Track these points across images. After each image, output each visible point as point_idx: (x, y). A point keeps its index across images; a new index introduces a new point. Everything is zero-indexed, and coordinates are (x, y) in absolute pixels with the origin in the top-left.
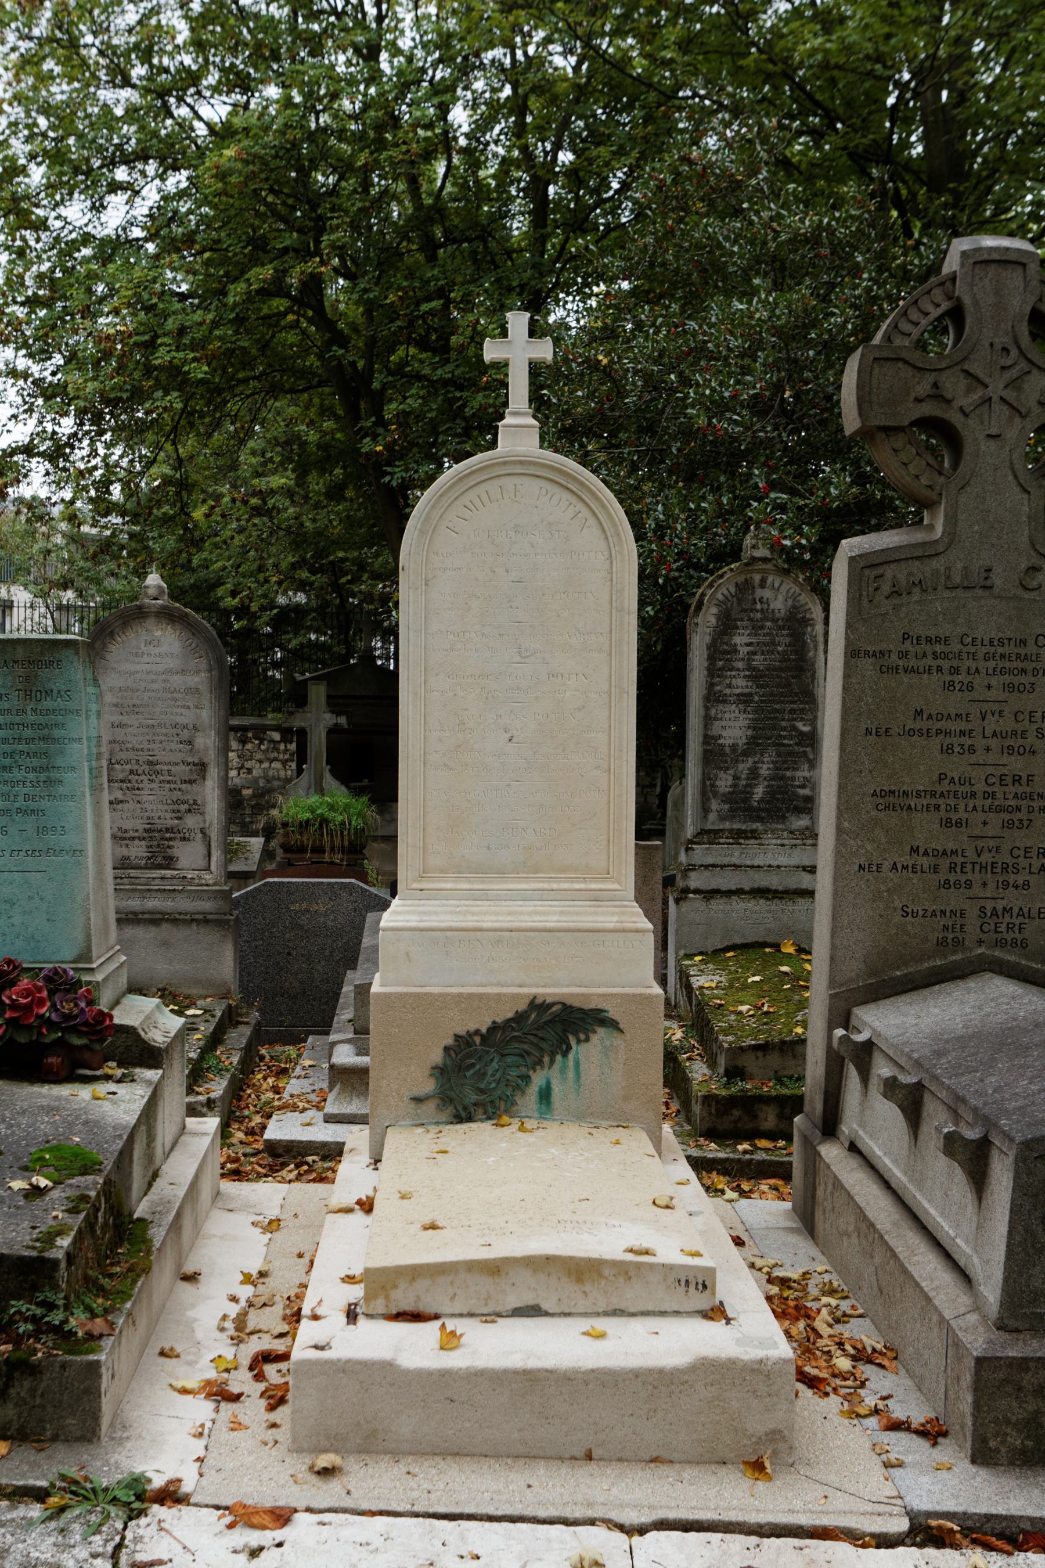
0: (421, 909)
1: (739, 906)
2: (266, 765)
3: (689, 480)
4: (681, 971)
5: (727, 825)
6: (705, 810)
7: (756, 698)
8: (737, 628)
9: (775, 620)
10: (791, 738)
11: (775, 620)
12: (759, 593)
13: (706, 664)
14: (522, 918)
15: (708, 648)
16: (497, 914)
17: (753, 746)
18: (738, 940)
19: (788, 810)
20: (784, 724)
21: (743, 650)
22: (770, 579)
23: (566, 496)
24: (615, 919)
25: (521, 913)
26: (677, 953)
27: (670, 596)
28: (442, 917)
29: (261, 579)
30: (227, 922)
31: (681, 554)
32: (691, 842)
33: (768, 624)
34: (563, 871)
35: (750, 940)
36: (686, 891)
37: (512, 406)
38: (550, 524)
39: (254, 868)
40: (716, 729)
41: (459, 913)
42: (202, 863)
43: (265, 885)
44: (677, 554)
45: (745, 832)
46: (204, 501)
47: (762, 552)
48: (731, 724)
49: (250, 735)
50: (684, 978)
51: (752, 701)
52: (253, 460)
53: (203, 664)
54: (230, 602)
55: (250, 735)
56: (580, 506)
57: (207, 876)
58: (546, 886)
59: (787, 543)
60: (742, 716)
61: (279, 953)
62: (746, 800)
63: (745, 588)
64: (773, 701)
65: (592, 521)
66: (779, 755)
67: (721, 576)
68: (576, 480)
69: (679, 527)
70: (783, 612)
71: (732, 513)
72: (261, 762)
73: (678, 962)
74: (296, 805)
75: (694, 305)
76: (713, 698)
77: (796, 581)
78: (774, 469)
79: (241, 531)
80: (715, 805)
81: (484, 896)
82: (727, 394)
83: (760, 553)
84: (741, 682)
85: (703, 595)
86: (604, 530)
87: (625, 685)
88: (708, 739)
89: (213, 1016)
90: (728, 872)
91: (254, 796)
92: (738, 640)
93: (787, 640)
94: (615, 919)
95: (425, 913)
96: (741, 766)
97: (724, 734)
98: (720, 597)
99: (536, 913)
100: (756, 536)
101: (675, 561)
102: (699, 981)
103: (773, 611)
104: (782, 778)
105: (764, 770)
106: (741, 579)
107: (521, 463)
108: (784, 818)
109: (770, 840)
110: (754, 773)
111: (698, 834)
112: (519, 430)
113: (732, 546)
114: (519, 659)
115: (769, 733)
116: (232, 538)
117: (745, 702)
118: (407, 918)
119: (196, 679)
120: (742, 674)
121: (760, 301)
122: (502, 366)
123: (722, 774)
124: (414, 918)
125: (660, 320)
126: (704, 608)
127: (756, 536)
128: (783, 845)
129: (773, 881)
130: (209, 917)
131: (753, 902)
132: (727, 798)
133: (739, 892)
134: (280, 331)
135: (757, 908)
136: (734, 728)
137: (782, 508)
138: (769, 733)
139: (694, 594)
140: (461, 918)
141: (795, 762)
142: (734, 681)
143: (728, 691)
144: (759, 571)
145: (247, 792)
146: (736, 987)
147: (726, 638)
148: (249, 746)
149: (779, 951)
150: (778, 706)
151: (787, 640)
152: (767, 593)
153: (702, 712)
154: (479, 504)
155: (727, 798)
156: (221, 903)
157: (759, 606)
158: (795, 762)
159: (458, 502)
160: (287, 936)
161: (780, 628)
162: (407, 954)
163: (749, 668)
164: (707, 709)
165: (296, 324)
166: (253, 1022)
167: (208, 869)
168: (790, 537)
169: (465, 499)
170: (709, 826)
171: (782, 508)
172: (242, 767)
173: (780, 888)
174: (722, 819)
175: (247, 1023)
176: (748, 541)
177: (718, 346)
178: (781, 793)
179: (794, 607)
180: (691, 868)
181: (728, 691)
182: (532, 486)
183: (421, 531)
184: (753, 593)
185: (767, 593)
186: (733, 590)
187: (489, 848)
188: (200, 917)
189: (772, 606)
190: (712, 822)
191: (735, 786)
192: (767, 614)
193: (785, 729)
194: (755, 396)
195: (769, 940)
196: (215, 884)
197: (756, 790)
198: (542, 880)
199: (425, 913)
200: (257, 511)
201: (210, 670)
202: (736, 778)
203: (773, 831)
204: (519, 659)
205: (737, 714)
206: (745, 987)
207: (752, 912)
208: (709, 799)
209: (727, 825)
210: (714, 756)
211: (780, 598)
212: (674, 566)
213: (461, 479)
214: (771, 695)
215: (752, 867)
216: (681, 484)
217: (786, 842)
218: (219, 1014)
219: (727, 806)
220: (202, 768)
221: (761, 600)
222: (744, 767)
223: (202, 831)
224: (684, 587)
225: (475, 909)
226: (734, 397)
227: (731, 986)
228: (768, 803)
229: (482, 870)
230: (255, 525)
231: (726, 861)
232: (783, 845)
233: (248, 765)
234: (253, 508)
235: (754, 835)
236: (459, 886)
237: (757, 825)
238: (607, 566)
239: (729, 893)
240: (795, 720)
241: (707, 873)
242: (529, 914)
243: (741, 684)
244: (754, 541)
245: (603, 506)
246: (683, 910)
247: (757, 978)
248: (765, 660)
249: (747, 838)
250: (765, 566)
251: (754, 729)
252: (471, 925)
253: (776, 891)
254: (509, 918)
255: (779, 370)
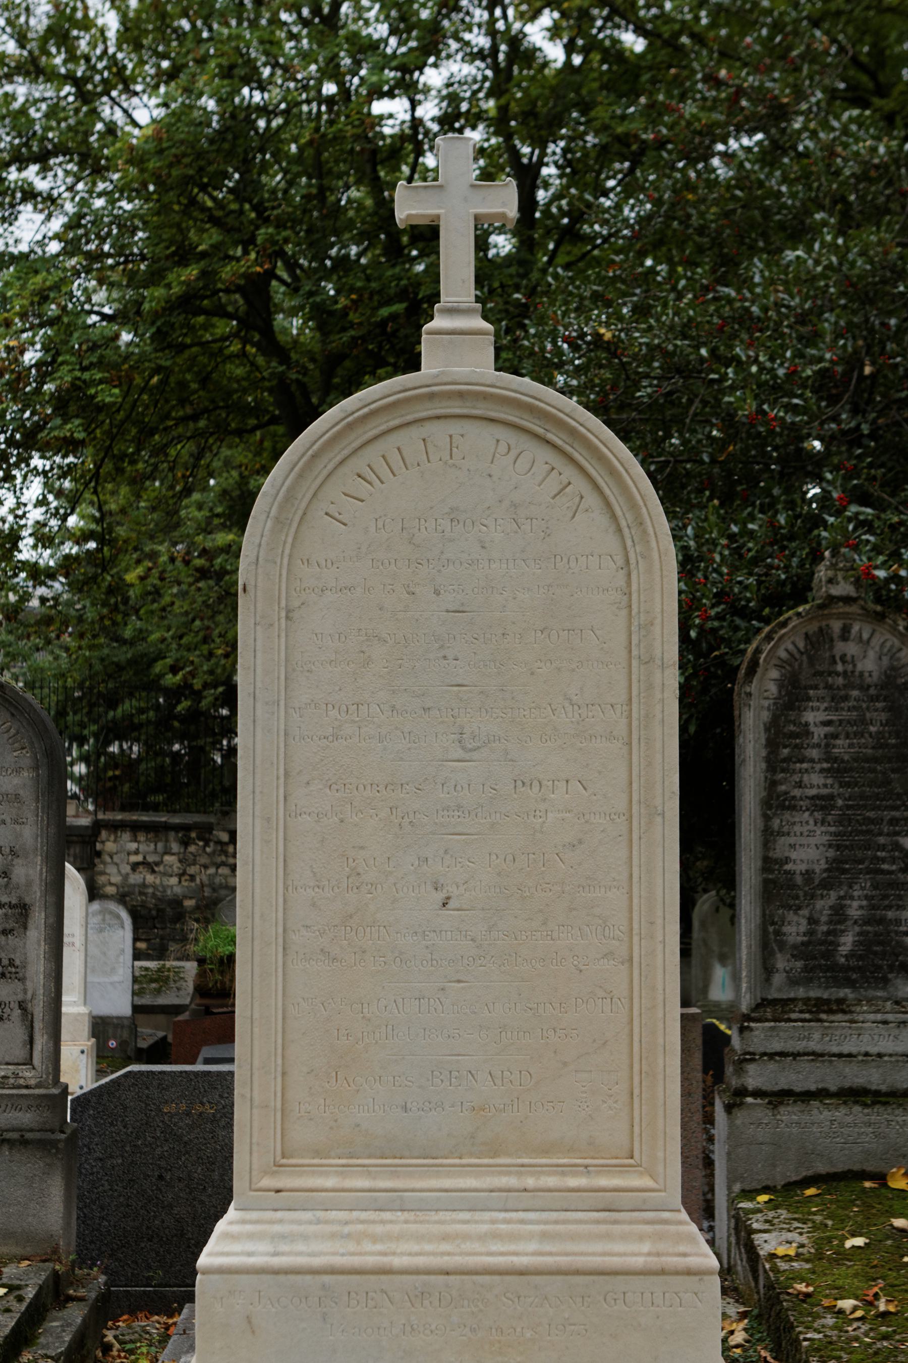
0: (277, 1228)
1: (822, 1116)
2: (212, 871)
3: (727, 499)
4: (737, 1218)
5: (801, 992)
6: (768, 970)
7: (840, 802)
8: (809, 699)
9: (864, 688)
10: (893, 861)
11: (864, 688)
12: (840, 647)
13: (764, 753)
14: (467, 1246)
15: (767, 729)
16: (419, 1238)
17: (838, 872)
18: (822, 1168)
19: (891, 968)
20: (882, 840)
21: (819, 732)
22: (856, 628)
23: (544, 455)
24: (646, 1247)
25: (466, 1237)
26: (729, 1188)
27: (706, 656)
28: (316, 1247)
29: (205, 652)
30: (54, 1144)
31: (720, 597)
32: (747, 1018)
33: (855, 693)
34: (545, 1151)
35: (840, 1168)
36: (742, 1092)
37: (446, 299)
38: (514, 505)
39: (187, 1001)
40: (781, 847)
41: (348, 1236)
42: (20, 1053)
43: (126, 1075)
44: (716, 595)
45: (828, 1002)
46: (139, 562)
47: (843, 588)
48: (804, 840)
49: (193, 835)
50: (743, 1235)
51: (833, 807)
52: (199, 515)
53: (26, 758)
54: (171, 680)
55: (193, 835)
56: (569, 473)
57: (28, 1074)
58: (512, 1181)
59: (881, 574)
60: (819, 830)
61: (147, 1176)
62: (829, 955)
63: (819, 640)
64: (865, 807)
65: (592, 499)
66: (875, 887)
67: (784, 624)
68: (560, 424)
69: (717, 558)
70: (875, 675)
71: (791, 538)
72: (206, 867)
73: (732, 1201)
74: (216, 936)
75: (728, 268)
76: (775, 802)
77: (894, 630)
78: (853, 473)
79: (183, 594)
80: (781, 962)
81: (396, 1201)
82: (781, 372)
83: (839, 590)
84: (816, 779)
85: (758, 651)
86: (614, 517)
87: (658, 801)
88: (769, 864)
89: (20, 1299)
90: (804, 1064)
91: (198, 907)
92: (810, 717)
93: (884, 716)
94: (646, 1247)
95: (283, 1237)
96: (819, 904)
97: (794, 855)
98: (783, 654)
99: (496, 1236)
100: (833, 566)
101: (713, 606)
102: (770, 1243)
103: (861, 674)
104: (882, 921)
105: (855, 910)
106: (813, 628)
107: (461, 395)
108: (885, 981)
109: (866, 1015)
110: (839, 914)
111: (758, 1006)
112: (457, 341)
113: (794, 584)
114: (460, 754)
115: (859, 854)
116: (173, 604)
117: (823, 808)
118: (250, 1246)
119: (16, 781)
120: (818, 767)
121: (823, 244)
122: (427, 236)
123: (791, 916)
124: (263, 1247)
125: (683, 282)
126: (760, 670)
127: (833, 566)
128: (885, 1022)
129: (873, 1078)
130: (29, 1136)
131: (843, 1110)
132: (801, 952)
133: (821, 1094)
134: (224, 362)
135: (849, 1119)
136: (808, 847)
137: (866, 525)
138: (859, 854)
139: (743, 652)
140: (352, 1247)
141: (900, 897)
142: (806, 778)
143: (797, 792)
144: (839, 616)
145: (189, 903)
146: (824, 1255)
147: (792, 715)
148: (192, 848)
149: (885, 1185)
150: (871, 814)
151: (884, 716)
152: (851, 649)
153: (760, 823)
154: (384, 472)
155: (801, 952)
156: (47, 1114)
157: (840, 668)
158: (900, 897)
159: (345, 469)
160: (158, 1151)
161: (872, 699)
162: (249, 1319)
163: (829, 757)
164: (767, 818)
165: (243, 354)
166: (93, 1295)
167: (29, 1062)
168: (884, 565)
169: (359, 463)
170: (774, 994)
171: (866, 525)
172: (184, 873)
173: (884, 1088)
174: (793, 982)
175: (81, 1299)
176: (822, 572)
177: (765, 309)
178: (880, 943)
179: (892, 668)
180: (749, 1057)
181: (797, 792)
182: (481, 438)
183: (277, 519)
184: (831, 648)
185: (851, 649)
186: (801, 645)
187: (405, 1109)
188: (15, 1135)
189: (859, 667)
190: (778, 988)
191: (810, 933)
192: (853, 679)
193: (883, 848)
194: (823, 374)
195: (869, 1167)
196: (38, 1086)
197: (843, 940)
198: (506, 1170)
199: (283, 1237)
200: (203, 573)
201: (36, 768)
202: (812, 921)
203: (869, 1001)
204: (460, 754)
205: (811, 826)
206: (843, 1256)
207: (842, 1125)
208: (772, 954)
209: (801, 992)
210: (778, 888)
211: (871, 654)
212: (713, 612)
213: (350, 426)
214: (862, 797)
215: (840, 1055)
216: (716, 502)
217: (890, 1017)
218: (30, 1293)
219: (799, 964)
220: (22, 911)
221: (843, 658)
222: (824, 905)
223: (22, 1005)
224: (728, 642)
225: (379, 1229)
226: (792, 374)
227: (819, 1256)
228: (861, 958)
229: (392, 1151)
230: (199, 589)
231: (800, 1046)
232: (885, 1022)
233: (192, 870)
234: (197, 570)
235: (840, 1007)
236: (349, 1183)
237: (846, 992)
238: (621, 582)
239: (806, 1096)
240: (898, 834)
241: (772, 1066)
242: (482, 1238)
243: (816, 782)
244: (830, 573)
245: (612, 472)
246: (738, 1122)
247: (859, 1241)
248: (851, 746)
249: (831, 1012)
250: (848, 609)
251: (838, 847)
252: (370, 1261)
253: (877, 1093)
254: (445, 1247)
255: (854, 338)
